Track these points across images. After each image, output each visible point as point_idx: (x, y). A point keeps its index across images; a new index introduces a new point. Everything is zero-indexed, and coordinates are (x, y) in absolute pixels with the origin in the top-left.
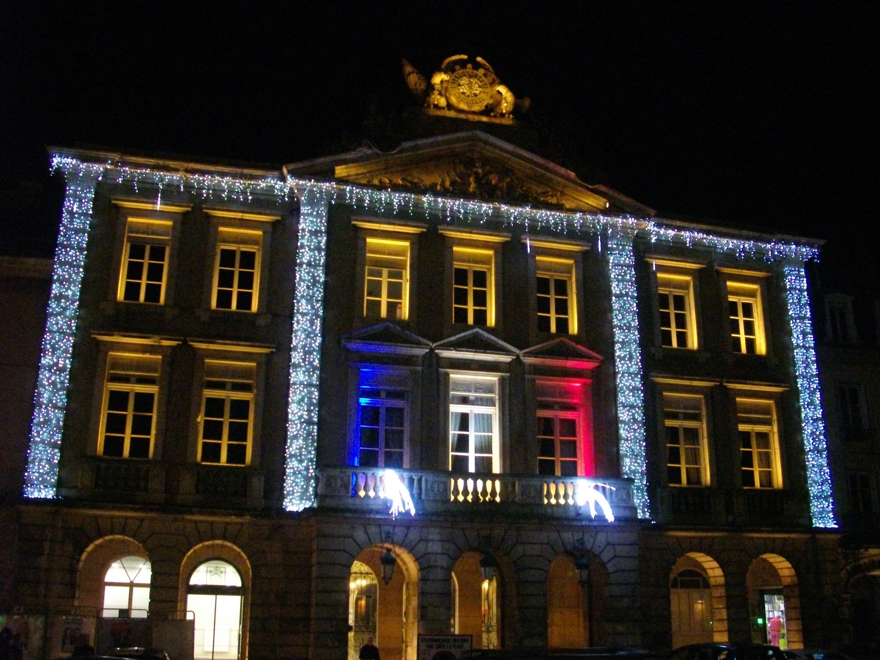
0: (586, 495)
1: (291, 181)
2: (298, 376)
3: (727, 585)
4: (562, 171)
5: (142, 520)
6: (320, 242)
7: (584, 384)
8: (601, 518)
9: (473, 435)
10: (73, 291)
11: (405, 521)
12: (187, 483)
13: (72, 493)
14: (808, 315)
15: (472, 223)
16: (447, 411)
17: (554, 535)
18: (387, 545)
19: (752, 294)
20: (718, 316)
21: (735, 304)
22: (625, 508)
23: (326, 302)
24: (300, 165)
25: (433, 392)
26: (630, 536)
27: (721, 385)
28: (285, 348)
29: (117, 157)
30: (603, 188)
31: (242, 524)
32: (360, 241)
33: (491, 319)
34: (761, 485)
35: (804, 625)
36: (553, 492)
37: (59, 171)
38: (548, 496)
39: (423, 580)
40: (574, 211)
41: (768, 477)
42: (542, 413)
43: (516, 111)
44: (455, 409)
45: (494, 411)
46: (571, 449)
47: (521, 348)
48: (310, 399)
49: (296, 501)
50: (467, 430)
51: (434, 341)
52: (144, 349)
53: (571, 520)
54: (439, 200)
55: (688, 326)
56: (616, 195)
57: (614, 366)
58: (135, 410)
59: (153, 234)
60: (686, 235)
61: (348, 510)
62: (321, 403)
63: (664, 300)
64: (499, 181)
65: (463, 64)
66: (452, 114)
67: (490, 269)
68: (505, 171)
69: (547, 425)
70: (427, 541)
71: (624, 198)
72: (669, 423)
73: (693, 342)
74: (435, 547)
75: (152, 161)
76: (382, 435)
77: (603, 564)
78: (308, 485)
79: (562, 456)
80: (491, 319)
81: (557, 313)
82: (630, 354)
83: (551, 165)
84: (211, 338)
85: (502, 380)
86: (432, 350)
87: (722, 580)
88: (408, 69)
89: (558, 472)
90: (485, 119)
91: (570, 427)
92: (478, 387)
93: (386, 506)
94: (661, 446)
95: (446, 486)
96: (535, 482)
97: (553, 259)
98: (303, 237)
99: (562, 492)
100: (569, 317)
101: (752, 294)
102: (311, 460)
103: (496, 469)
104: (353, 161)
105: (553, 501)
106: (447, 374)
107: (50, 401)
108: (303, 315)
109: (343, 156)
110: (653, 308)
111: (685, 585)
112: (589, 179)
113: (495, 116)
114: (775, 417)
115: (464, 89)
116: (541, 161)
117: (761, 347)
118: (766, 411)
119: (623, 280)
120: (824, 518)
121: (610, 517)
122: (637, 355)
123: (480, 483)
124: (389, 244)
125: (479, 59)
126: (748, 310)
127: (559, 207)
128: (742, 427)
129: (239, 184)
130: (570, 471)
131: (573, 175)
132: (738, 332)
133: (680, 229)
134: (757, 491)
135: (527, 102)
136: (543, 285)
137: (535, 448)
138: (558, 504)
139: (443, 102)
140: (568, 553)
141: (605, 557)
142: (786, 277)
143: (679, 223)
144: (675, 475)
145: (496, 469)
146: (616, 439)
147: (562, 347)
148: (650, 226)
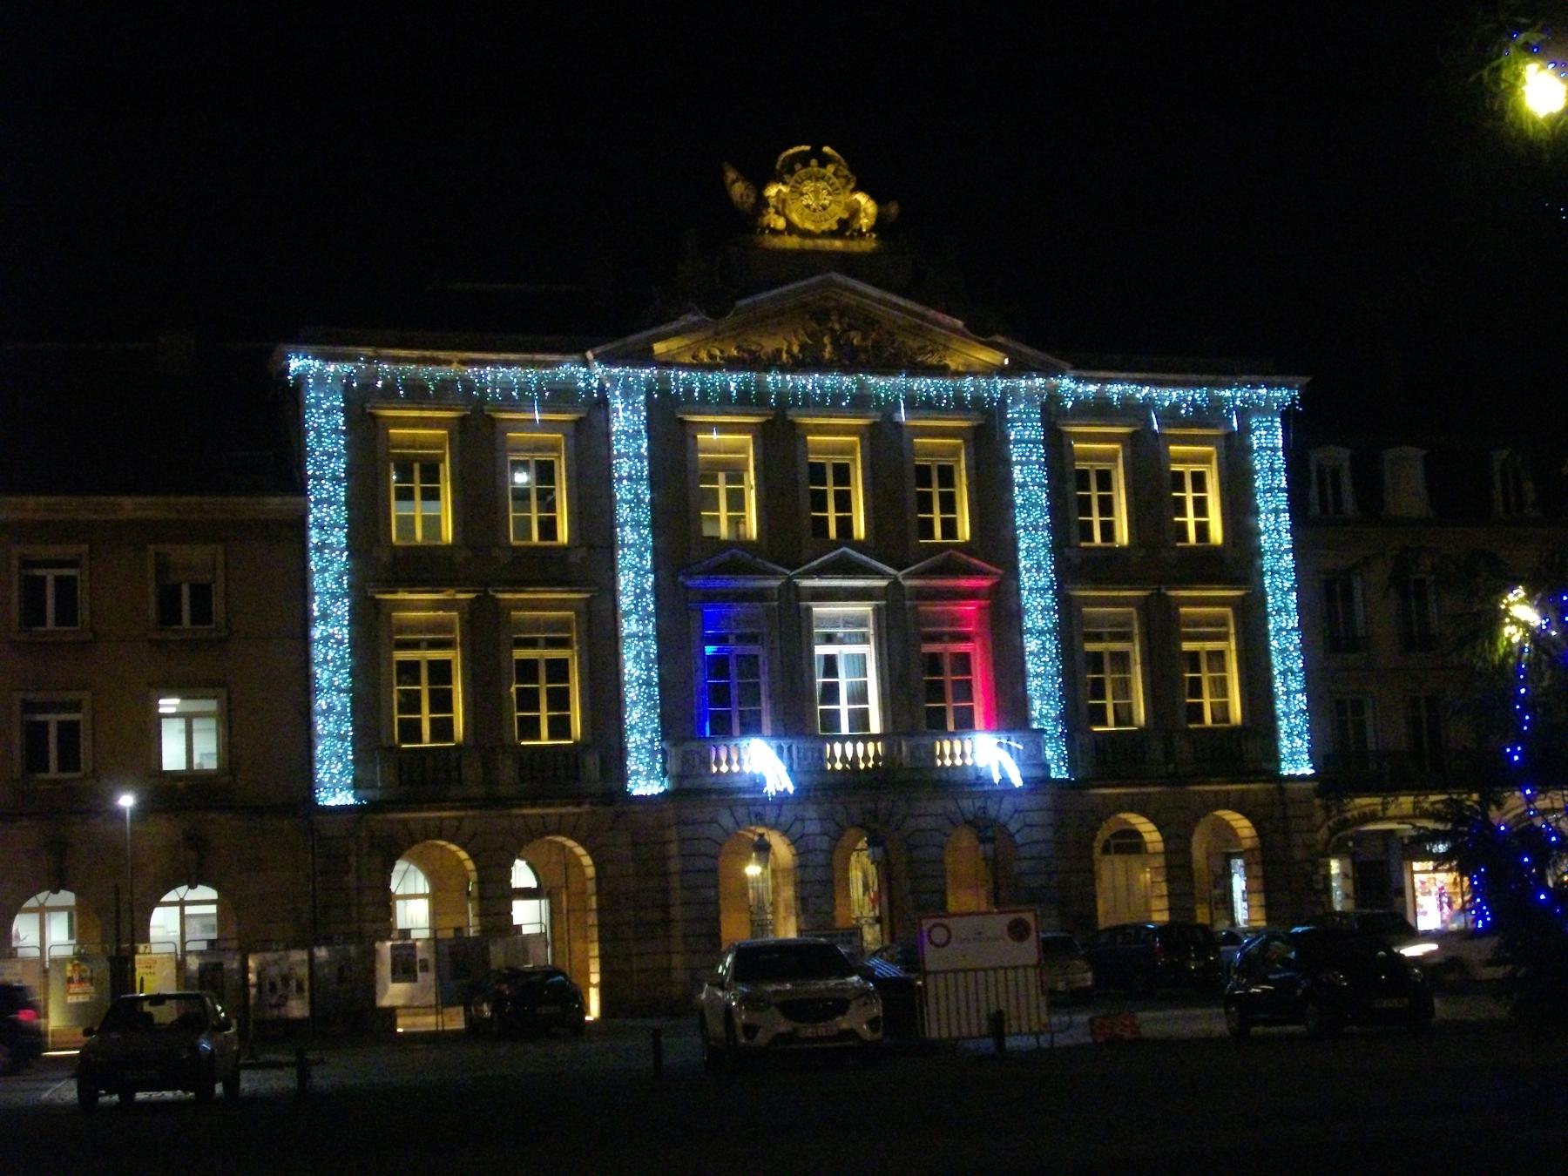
0: (987, 754)
1: (599, 370)
2: (629, 626)
3: (1167, 852)
4: (947, 319)
5: (460, 819)
6: (640, 447)
7: (980, 607)
8: (1005, 780)
9: (844, 682)
10: (339, 537)
11: (782, 799)
12: (508, 771)
13: (376, 794)
14: (1284, 484)
15: (831, 403)
16: (811, 651)
17: (951, 806)
18: (761, 830)
19: (1205, 459)
20: (1156, 494)
21: (1180, 475)
22: (1035, 765)
23: (655, 527)
24: (609, 347)
25: (794, 630)
26: (1046, 800)
27: (1159, 594)
28: (610, 591)
29: (369, 351)
30: (1000, 339)
31: (579, 815)
32: (690, 440)
33: (860, 530)
34: (1214, 720)
35: (1267, 898)
36: (947, 752)
37: (301, 378)
38: (942, 756)
39: (802, 866)
40: (960, 374)
41: (1222, 711)
42: (928, 648)
43: (880, 226)
44: (821, 650)
45: (869, 650)
46: (965, 691)
47: (900, 569)
48: (647, 654)
49: (645, 784)
50: (836, 675)
51: (792, 569)
52: (437, 606)
53: (970, 784)
54: (788, 377)
55: (1116, 512)
56: (1019, 346)
57: (1017, 579)
58: (431, 682)
59: (422, 447)
60: (1115, 390)
61: (710, 791)
62: (661, 658)
63: (1082, 479)
64: (864, 339)
65: (804, 159)
66: (793, 242)
67: (854, 460)
68: (868, 323)
69: (934, 663)
70: (803, 820)
71: (1027, 350)
72: (1091, 647)
73: (1123, 536)
74: (813, 827)
75: (416, 353)
76: (734, 693)
77: (1011, 836)
78: (655, 760)
79: (955, 701)
80: (860, 530)
81: (942, 512)
82: (1039, 563)
83: (932, 313)
84: (517, 584)
85: (877, 610)
86: (790, 578)
87: (1160, 847)
88: (731, 175)
89: (951, 727)
90: (838, 244)
91: (963, 661)
92: (847, 622)
93: (757, 785)
94: (1079, 711)
95: (822, 751)
96: (926, 741)
97: (937, 441)
98: (619, 441)
99: (958, 751)
100: (958, 516)
101: (1205, 459)
102: (655, 730)
103: (875, 727)
104: (677, 333)
105: (948, 762)
106: (809, 609)
107: (331, 684)
108: (630, 546)
109: (663, 329)
110: (1069, 488)
111: (1121, 850)
112: (981, 332)
113: (852, 237)
114: (1232, 631)
115: (809, 200)
116: (917, 308)
117: (1216, 534)
118: (1221, 621)
119: (1028, 463)
120: (1296, 761)
121: (1018, 782)
122: (1048, 564)
123: (860, 746)
124: (724, 441)
125: (827, 149)
126: (1199, 481)
127: (941, 371)
128: (1187, 646)
129: (531, 374)
130: (965, 724)
131: (960, 324)
132: (1184, 515)
133: (1104, 381)
134: (1208, 730)
135: (894, 209)
136: (923, 475)
137: (923, 692)
138: (953, 766)
139: (780, 223)
140: (968, 822)
141: (1013, 827)
142: (1252, 432)
143: (1102, 374)
144: (1099, 715)
145: (875, 727)
146: (1022, 674)
147: (950, 562)
148: (1066, 383)
